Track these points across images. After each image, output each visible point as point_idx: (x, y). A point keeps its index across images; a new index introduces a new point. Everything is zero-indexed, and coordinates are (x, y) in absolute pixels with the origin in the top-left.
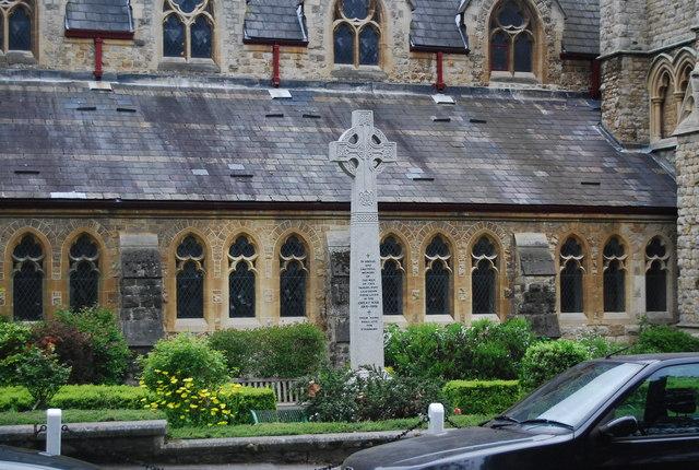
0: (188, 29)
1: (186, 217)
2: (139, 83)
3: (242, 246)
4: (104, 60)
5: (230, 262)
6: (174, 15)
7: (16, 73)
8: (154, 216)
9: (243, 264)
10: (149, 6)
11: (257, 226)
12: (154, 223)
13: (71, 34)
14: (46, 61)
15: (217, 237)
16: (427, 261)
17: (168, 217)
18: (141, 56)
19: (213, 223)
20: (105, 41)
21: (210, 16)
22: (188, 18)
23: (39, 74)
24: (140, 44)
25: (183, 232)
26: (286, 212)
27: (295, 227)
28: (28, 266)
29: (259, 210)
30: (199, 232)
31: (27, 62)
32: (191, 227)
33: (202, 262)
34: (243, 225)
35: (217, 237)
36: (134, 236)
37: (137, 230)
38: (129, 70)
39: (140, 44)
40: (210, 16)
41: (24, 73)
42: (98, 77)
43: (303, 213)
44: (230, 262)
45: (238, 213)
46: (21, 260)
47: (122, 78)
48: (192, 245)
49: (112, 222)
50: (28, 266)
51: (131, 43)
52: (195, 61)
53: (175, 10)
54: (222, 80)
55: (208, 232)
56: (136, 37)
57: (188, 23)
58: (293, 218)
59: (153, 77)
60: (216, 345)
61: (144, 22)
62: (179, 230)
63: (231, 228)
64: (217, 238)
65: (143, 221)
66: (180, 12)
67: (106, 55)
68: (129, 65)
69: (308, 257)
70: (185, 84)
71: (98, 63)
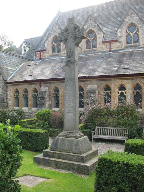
0: (132, 37)
1: (105, 80)
2: (119, 51)
3: (122, 88)
4: (111, 47)
5: (118, 92)
6: (129, 34)
7: (92, 53)
8: (97, 80)
9: (122, 93)
10: (122, 33)
11: (126, 81)
12: (97, 82)
13: (104, 42)
14: (99, 50)
15: (115, 85)
16: (134, 92)
17: (100, 80)
18: (120, 45)
19: (113, 81)
20: (111, 43)
21: (138, 33)
22: (132, 34)
23: (97, 53)
24: (120, 42)
25: (105, 84)
26: (134, 77)
27: (137, 81)
28: (138, 93)
29: (126, 77)
30: (109, 84)
31: (96, 50)
32: (107, 83)
33: (141, 92)
34: (122, 81)
35: (115, 85)
36: (91, 86)
37: (93, 84)
38: (117, 49)
39: (120, 42)
40: (138, 33)
41: (94, 53)
42: (110, 51)
43: (139, 77)
44: (118, 92)
45: (119, 78)
46: (136, 91)
47: (115, 51)
48: (108, 88)
49: (86, 82)
50: (138, 93)
51: (118, 42)
52: (134, 44)
53: (129, 33)
54: (141, 48)
55: (112, 84)
56: (119, 41)
57: (132, 35)
58: (137, 79)
59: (123, 50)
60: (18, 137)
61: (120, 37)
62: (103, 84)
63: (118, 83)
64: (114, 86)
65: (94, 82)
66: (130, 33)
67: (112, 46)
68: (117, 48)
69: (142, 91)
70: (131, 50)
71: (110, 48)
